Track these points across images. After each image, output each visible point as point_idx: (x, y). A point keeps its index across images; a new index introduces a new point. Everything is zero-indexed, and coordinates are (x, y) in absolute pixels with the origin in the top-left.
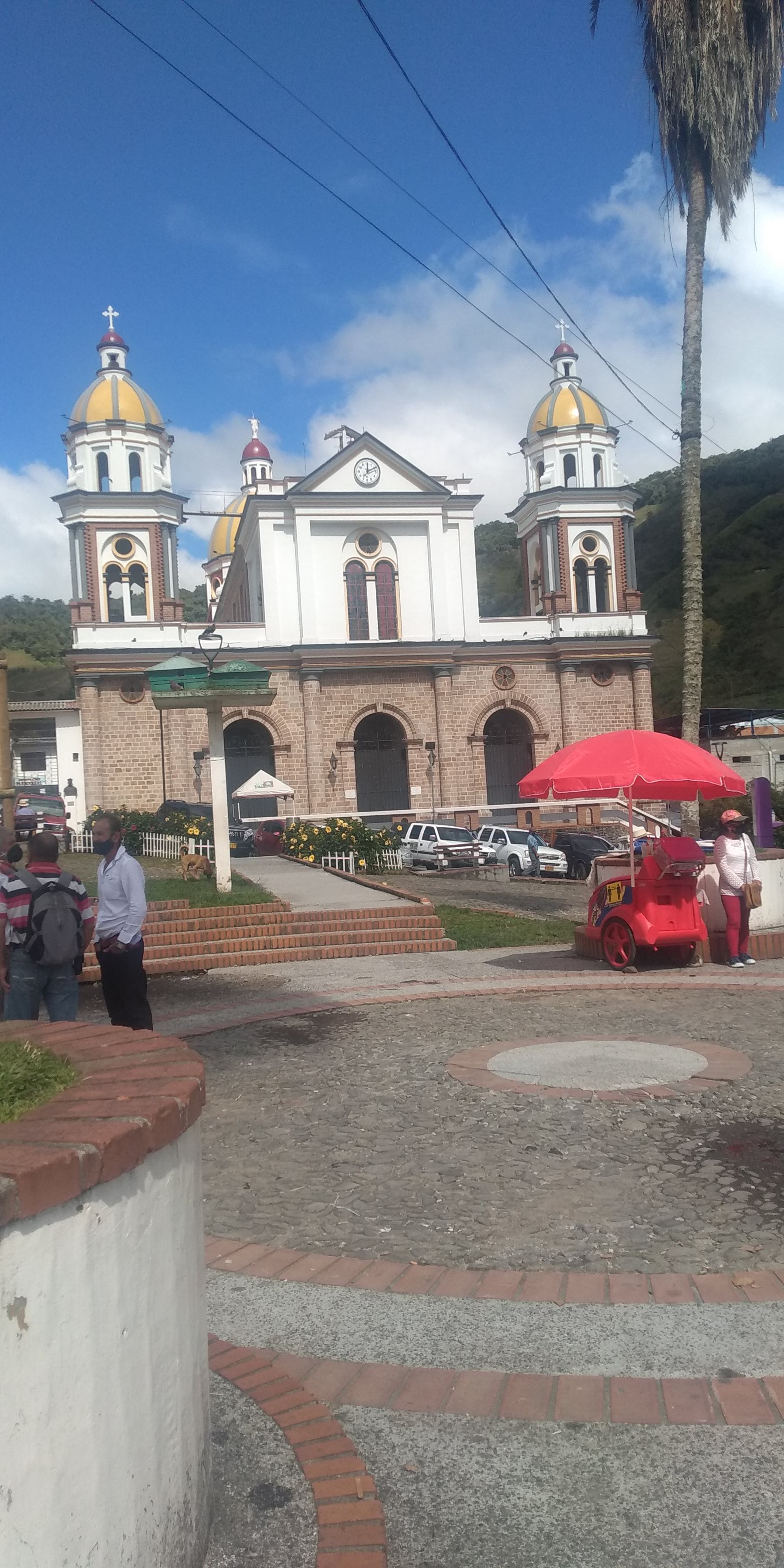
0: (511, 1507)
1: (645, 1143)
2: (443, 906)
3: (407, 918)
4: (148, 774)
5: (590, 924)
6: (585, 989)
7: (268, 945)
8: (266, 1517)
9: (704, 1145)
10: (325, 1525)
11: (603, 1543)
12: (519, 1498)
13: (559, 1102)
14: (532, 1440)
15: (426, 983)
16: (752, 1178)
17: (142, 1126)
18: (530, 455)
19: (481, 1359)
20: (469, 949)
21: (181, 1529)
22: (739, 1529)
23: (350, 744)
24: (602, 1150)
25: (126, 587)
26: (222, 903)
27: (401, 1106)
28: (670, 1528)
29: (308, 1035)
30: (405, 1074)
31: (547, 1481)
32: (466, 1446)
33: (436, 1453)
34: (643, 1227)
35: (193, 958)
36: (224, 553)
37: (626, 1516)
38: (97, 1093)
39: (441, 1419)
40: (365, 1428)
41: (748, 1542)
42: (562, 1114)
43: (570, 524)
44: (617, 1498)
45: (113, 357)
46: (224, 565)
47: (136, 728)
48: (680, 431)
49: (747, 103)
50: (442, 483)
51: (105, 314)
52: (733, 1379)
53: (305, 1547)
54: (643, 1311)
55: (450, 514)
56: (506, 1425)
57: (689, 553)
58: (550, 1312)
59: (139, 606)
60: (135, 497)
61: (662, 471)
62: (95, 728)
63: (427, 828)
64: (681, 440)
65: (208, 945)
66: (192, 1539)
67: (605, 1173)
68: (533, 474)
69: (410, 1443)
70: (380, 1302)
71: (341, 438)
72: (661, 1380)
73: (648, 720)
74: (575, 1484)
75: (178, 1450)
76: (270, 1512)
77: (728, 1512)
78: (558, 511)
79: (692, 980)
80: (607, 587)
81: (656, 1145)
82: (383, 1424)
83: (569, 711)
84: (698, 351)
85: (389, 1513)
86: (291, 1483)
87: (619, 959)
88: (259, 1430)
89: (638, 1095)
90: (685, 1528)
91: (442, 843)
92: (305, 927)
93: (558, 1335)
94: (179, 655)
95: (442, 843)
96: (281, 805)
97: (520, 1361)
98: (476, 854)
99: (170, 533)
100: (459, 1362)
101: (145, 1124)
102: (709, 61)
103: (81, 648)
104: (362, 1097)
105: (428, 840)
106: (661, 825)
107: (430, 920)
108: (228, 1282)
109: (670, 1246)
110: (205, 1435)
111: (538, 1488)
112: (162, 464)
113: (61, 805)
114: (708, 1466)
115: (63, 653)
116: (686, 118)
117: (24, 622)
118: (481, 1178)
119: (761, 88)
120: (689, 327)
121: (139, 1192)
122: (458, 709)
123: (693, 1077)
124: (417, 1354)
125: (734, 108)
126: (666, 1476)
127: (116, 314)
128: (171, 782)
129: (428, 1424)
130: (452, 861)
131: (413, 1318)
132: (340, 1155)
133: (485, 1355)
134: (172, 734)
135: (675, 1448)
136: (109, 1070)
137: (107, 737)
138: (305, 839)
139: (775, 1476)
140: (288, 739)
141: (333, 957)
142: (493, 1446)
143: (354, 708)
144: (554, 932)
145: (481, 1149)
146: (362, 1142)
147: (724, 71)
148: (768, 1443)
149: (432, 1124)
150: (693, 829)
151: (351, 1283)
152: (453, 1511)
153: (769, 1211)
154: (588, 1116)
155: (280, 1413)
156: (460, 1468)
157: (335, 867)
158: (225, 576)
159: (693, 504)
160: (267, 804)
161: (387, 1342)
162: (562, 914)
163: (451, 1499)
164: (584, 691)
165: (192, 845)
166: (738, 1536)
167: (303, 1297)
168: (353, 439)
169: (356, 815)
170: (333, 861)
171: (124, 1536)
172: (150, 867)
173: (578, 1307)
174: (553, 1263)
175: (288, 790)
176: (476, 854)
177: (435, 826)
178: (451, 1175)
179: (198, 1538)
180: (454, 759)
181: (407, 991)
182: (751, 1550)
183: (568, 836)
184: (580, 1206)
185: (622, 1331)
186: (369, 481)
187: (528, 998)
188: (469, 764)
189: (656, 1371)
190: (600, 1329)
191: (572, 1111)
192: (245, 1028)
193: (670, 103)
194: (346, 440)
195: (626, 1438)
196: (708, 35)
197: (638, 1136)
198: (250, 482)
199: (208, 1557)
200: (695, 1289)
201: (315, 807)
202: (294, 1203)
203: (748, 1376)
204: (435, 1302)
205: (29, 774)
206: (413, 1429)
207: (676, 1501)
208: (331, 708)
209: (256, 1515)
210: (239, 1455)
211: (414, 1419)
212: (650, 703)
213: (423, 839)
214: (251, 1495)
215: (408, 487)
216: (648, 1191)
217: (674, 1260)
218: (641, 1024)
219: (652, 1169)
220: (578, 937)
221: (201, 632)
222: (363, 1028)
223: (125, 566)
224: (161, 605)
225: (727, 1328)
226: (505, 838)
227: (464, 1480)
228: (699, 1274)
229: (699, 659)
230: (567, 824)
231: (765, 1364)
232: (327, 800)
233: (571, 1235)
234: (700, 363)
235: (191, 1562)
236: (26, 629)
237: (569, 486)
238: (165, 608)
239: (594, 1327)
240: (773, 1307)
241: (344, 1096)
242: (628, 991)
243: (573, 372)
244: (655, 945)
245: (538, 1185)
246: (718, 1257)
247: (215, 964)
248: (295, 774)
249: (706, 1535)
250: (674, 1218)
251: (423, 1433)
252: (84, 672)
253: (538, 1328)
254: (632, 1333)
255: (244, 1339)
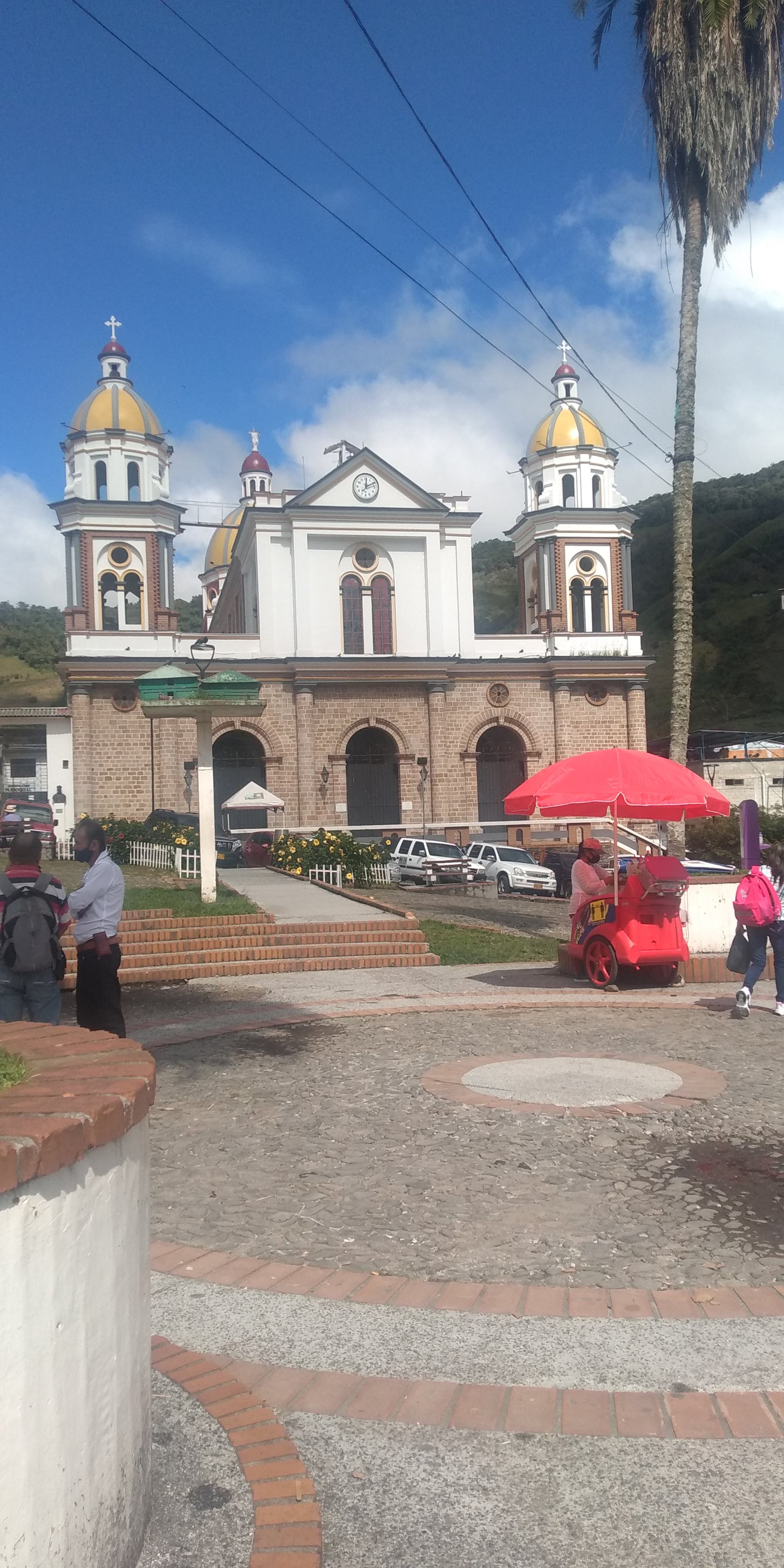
0: (455, 1514)
1: (615, 1160)
2: (428, 921)
3: (391, 932)
4: (138, 783)
5: (573, 941)
6: (565, 1006)
7: (250, 957)
8: (203, 1517)
9: (673, 1163)
10: (261, 1527)
11: (545, 1552)
12: (464, 1507)
13: (531, 1118)
14: (482, 1450)
15: (407, 998)
16: (719, 1197)
17: (83, 1121)
18: (529, 475)
19: (436, 1369)
20: (452, 964)
21: (114, 1525)
22: (681, 1541)
23: (341, 758)
24: (571, 1166)
25: (121, 595)
26: (206, 914)
27: (373, 1118)
28: (613, 1539)
29: (285, 1047)
30: (379, 1086)
31: (493, 1490)
32: (414, 1455)
33: (384, 1461)
34: (606, 1242)
35: (175, 967)
36: (221, 564)
37: (570, 1526)
38: (45, 1090)
39: (392, 1427)
40: (315, 1435)
41: (689, 1554)
42: (534, 1129)
43: (567, 544)
44: (562, 1508)
45: (114, 367)
46: (221, 576)
47: (127, 736)
48: (673, 454)
49: (745, 133)
50: (440, 500)
51: (108, 324)
52: (685, 1393)
53: (241, 1547)
54: (601, 1325)
55: (448, 531)
56: (456, 1434)
57: (680, 575)
58: (507, 1324)
59: (133, 614)
60: (133, 507)
61: (662, 494)
62: (86, 736)
63: (417, 843)
64: (674, 463)
65: (190, 955)
66: (126, 1536)
67: (572, 1189)
68: (532, 493)
69: (360, 1450)
70: (338, 1311)
71: (341, 453)
72: (613, 1394)
73: (642, 740)
74: (521, 1493)
75: (113, 1446)
76: (207, 1513)
77: (672, 1523)
78: (556, 531)
79: (673, 1000)
80: (603, 607)
81: (625, 1163)
82: (334, 1432)
83: (562, 730)
84: (693, 375)
85: (332, 1517)
86: (231, 1485)
87: (602, 978)
88: (203, 1432)
89: (611, 1112)
90: (627, 1538)
91: (431, 858)
92: (288, 939)
93: (514, 1346)
94: (170, 664)
95: (431, 858)
96: (271, 816)
97: (475, 1372)
98: (465, 870)
99: (167, 542)
100: (413, 1372)
101: (87, 1120)
102: (707, 90)
103: (73, 655)
104: (335, 1108)
105: (418, 855)
106: (652, 845)
107: (415, 934)
108: (187, 1289)
109: (632, 1262)
110: (144, 1433)
111: (484, 1498)
112: (160, 474)
113: (49, 811)
114: (654, 1479)
115: (56, 660)
116: (684, 146)
117: (18, 628)
118: (448, 1191)
119: (758, 118)
120: (684, 351)
121: (79, 1187)
122: (451, 725)
123: (666, 1096)
124: (371, 1363)
125: (732, 137)
126: (611, 1487)
127: (119, 324)
128: (161, 791)
129: (378, 1432)
130: (440, 876)
131: (370, 1327)
132: (309, 1166)
133: (440, 1365)
134: (163, 743)
135: (623, 1460)
136: (60, 1068)
137: (98, 745)
138: (293, 852)
139: (720, 1489)
140: (280, 751)
141: (316, 970)
142: (442, 1455)
143: (347, 722)
144: (538, 950)
145: (450, 1162)
146: (332, 1153)
147: (723, 101)
148: (716, 1457)
149: (404, 1136)
150: (678, 849)
151: (311, 1292)
152: (397, 1518)
153: (734, 1229)
154: (559, 1131)
155: (226, 1415)
156: (407, 1475)
157: (322, 880)
158: (221, 588)
159: (684, 527)
160: (257, 816)
161: (343, 1351)
162: (547, 932)
163: (396, 1506)
164: (578, 711)
165: (179, 854)
166: (680, 1547)
167: (262, 1305)
168: (352, 454)
169: (346, 829)
170: (321, 874)
171: (53, 1529)
172: (136, 875)
173: (536, 1320)
174: (514, 1276)
175: (279, 802)
176: (465, 870)
177: (424, 842)
178: (418, 1187)
179: (132, 1535)
180: (446, 775)
181: (388, 1005)
182: (691, 1561)
183: (558, 855)
184: (545, 1220)
185: (578, 1344)
186: (368, 497)
187: (508, 1014)
188: (461, 780)
189: (609, 1384)
190: (556, 1341)
191: (543, 1126)
192: (223, 1038)
193: (668, 131)
194: (346, 455)
195: (575, 1449)
196: (706, 66)
197: (607, 1152)
198: (249, 494)
199: (143, 1555)
200: (653, 1304)
201: (305, 820)
202: (259, 1212)
203: (701, 1390)
204: (393, 1313)
205: (18, 781)
206: (363, 1436)
207: (621, 1512)
208: (324, 721)
209: (193, 1515)
210: (181, 1455)
211: (364, 1427)
212: (644, 723)
213: (412, 854)
214: (190, 1495)
215: (406, 502)
216: (614, 1207)
217: (634, 1276)
218: (619, 1042)
219: (620, 1186)
220: (562, 954)
221: (194, 642)
222: (340, 1041)
223: (120, 574)
224: (156, 615)
225: (684, 1344)
226: (495, 855)
227: (410, 1488)
228: (659, 1289)
229: (688, 680)
230: (557, 843)
231: (719, 1379)
232: (318, 813)
233: (534, 1248)
234: (694, 387)
235: (124, 1558)
236: (20, 635)
237: (567, 506)
238: (160, 617)
239: (551, 1339)
240: (730, 1324)
241: (317, 1107)
242: (608, 1009)
243: (574, 393)
244: (637, 964)
245: (504, 1199)
246: (679, 1273)
247: (196, 974)
248: (286, 786)
249: (647, 1546)
250: (638, 1234)
251: (373, 1441)
252: (75, 680)
253: (495, 1340)
254: (588, 1346)
255: (200, 1345)
